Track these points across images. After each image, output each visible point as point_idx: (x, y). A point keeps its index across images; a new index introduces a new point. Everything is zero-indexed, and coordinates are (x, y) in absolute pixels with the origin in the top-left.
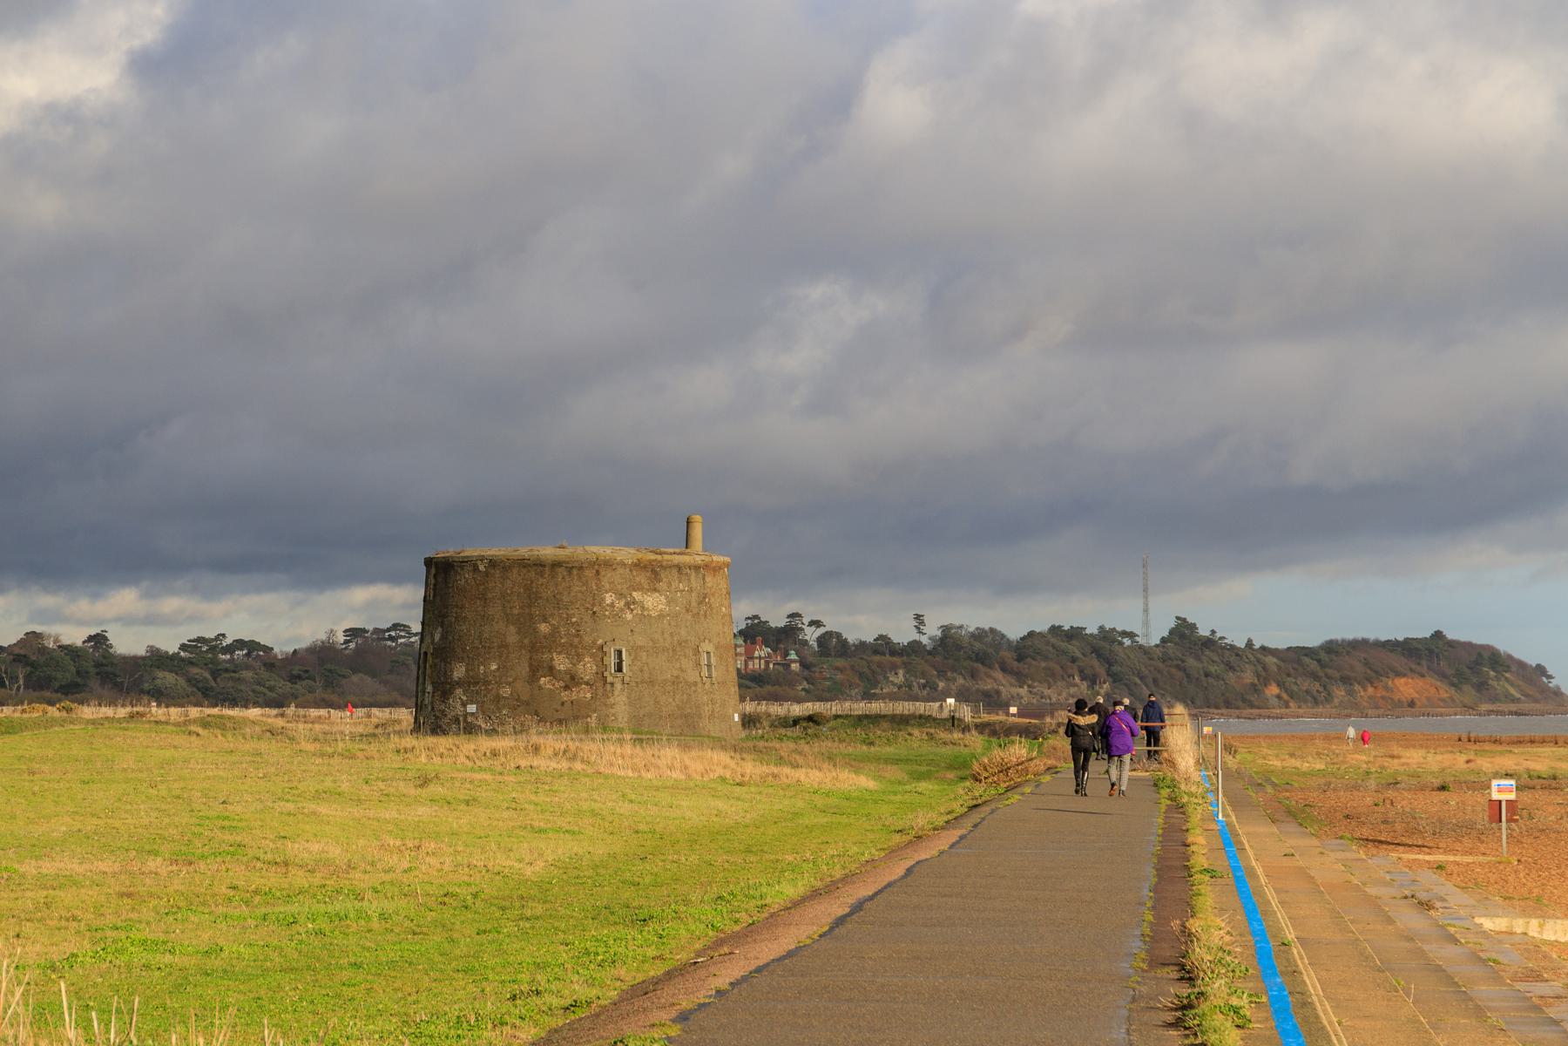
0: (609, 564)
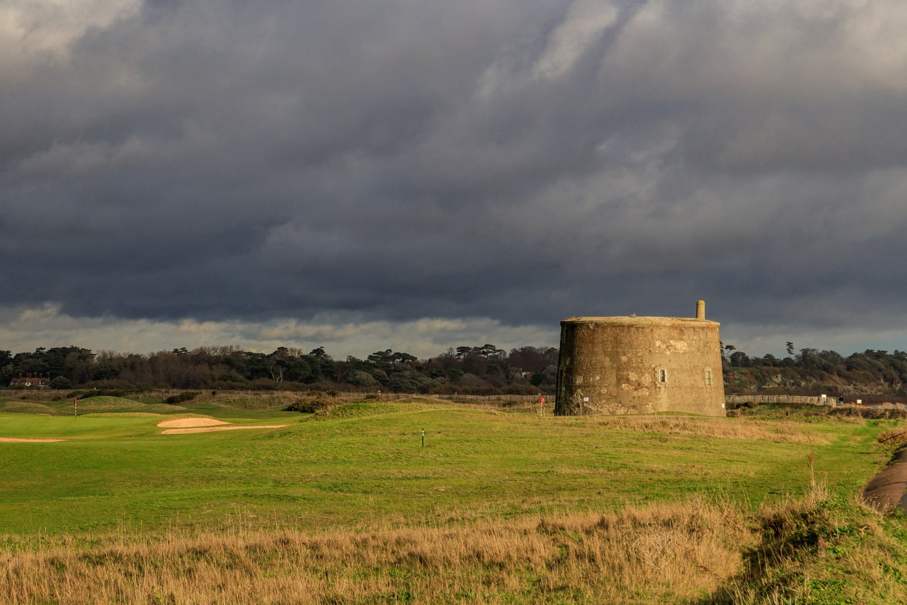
0: (657, 326)
